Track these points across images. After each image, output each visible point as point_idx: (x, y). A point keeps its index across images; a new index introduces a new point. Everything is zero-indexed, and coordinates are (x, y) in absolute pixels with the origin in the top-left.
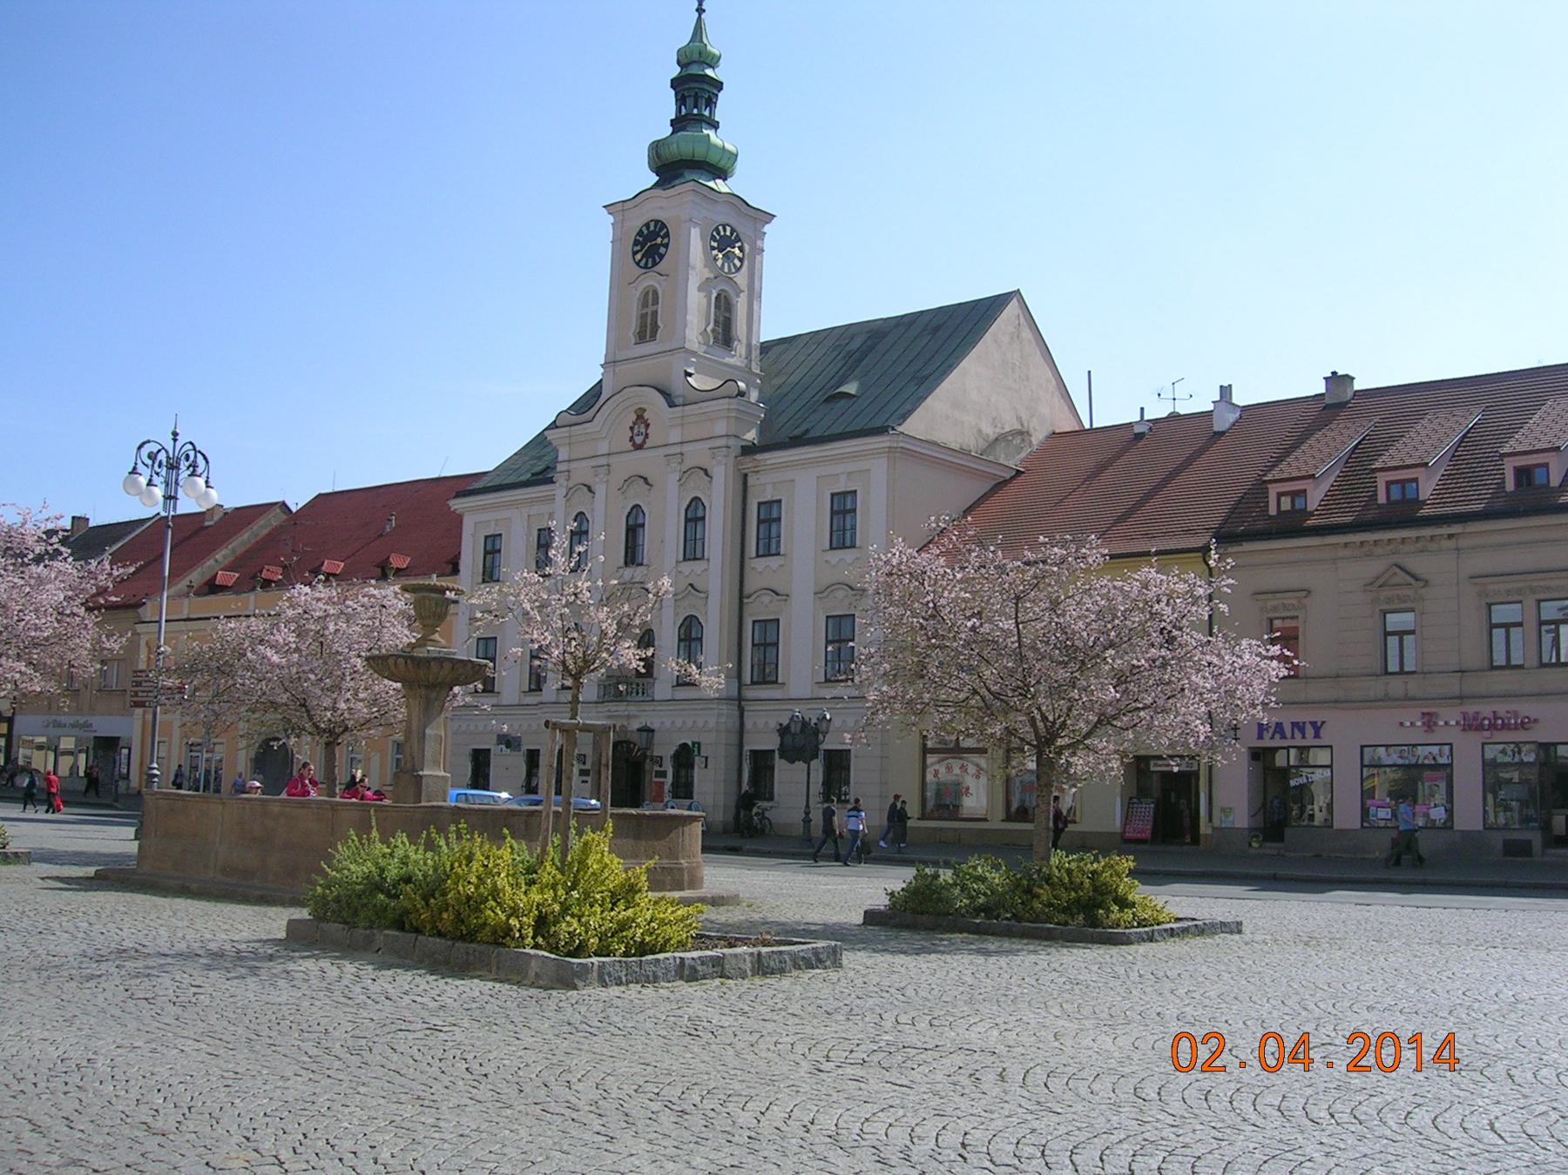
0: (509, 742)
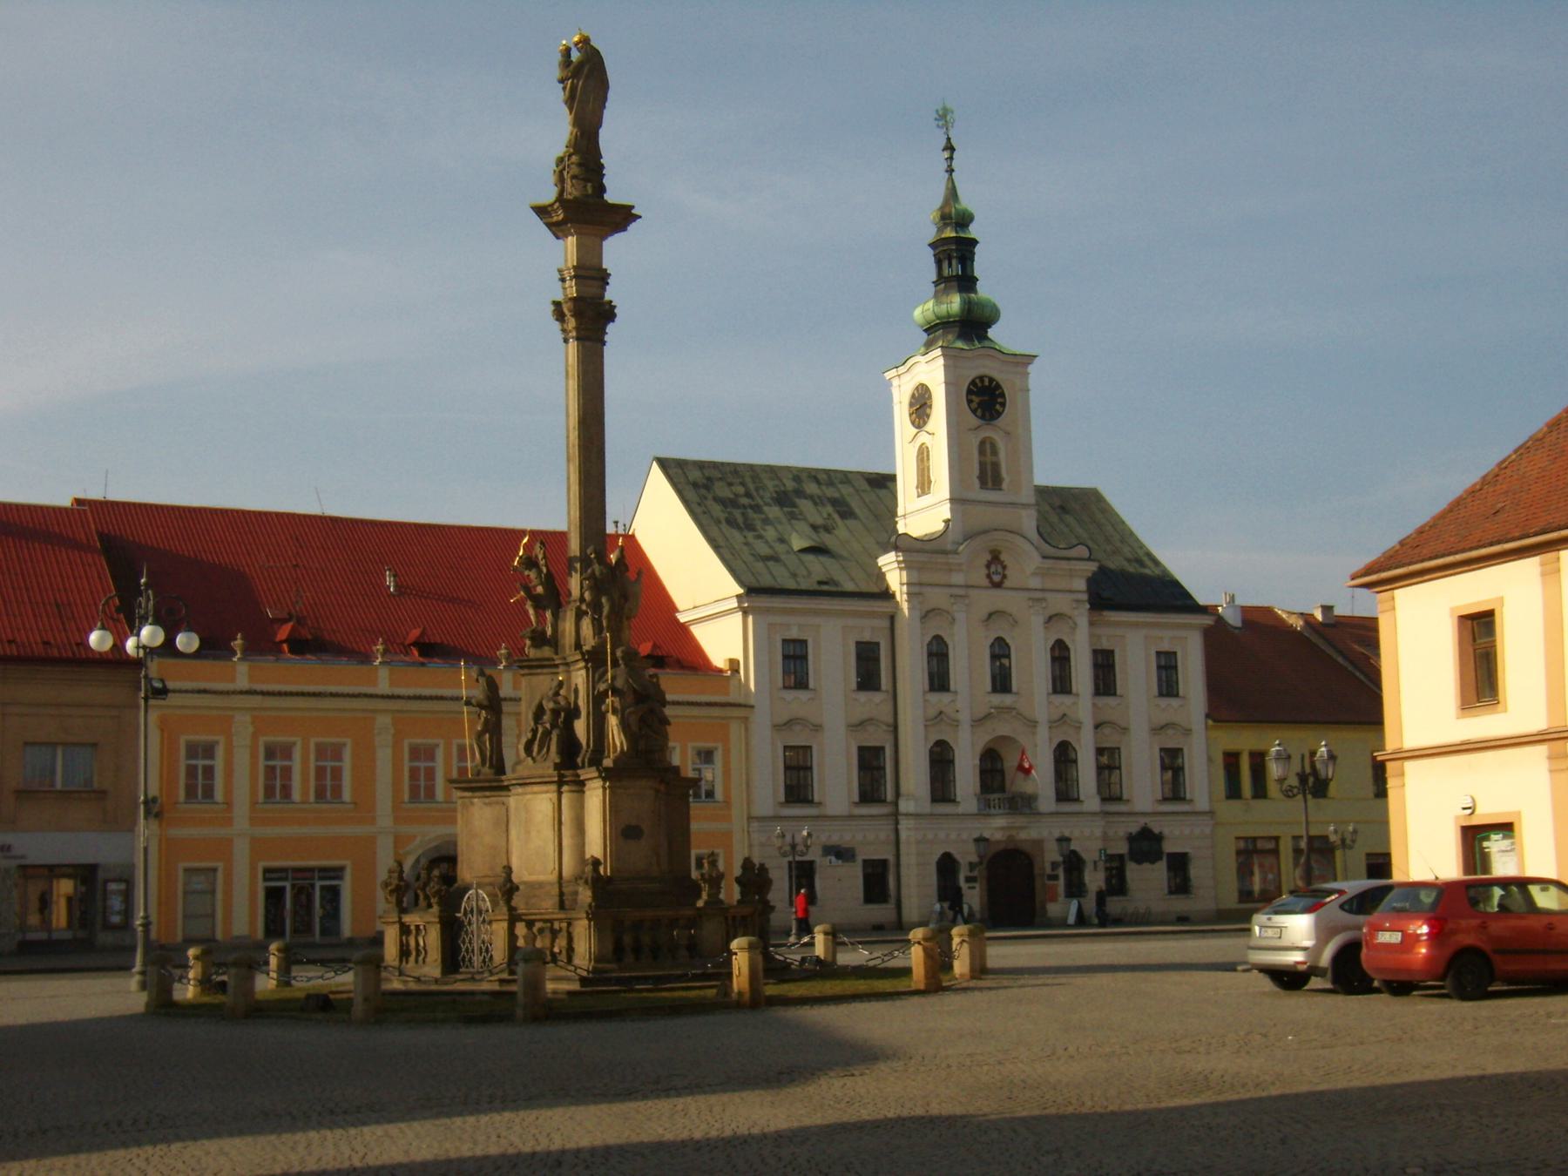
0: (843, 854)
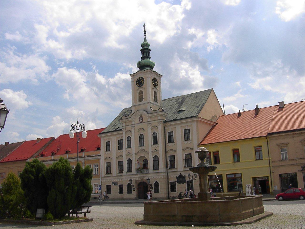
0: (115, 183)
